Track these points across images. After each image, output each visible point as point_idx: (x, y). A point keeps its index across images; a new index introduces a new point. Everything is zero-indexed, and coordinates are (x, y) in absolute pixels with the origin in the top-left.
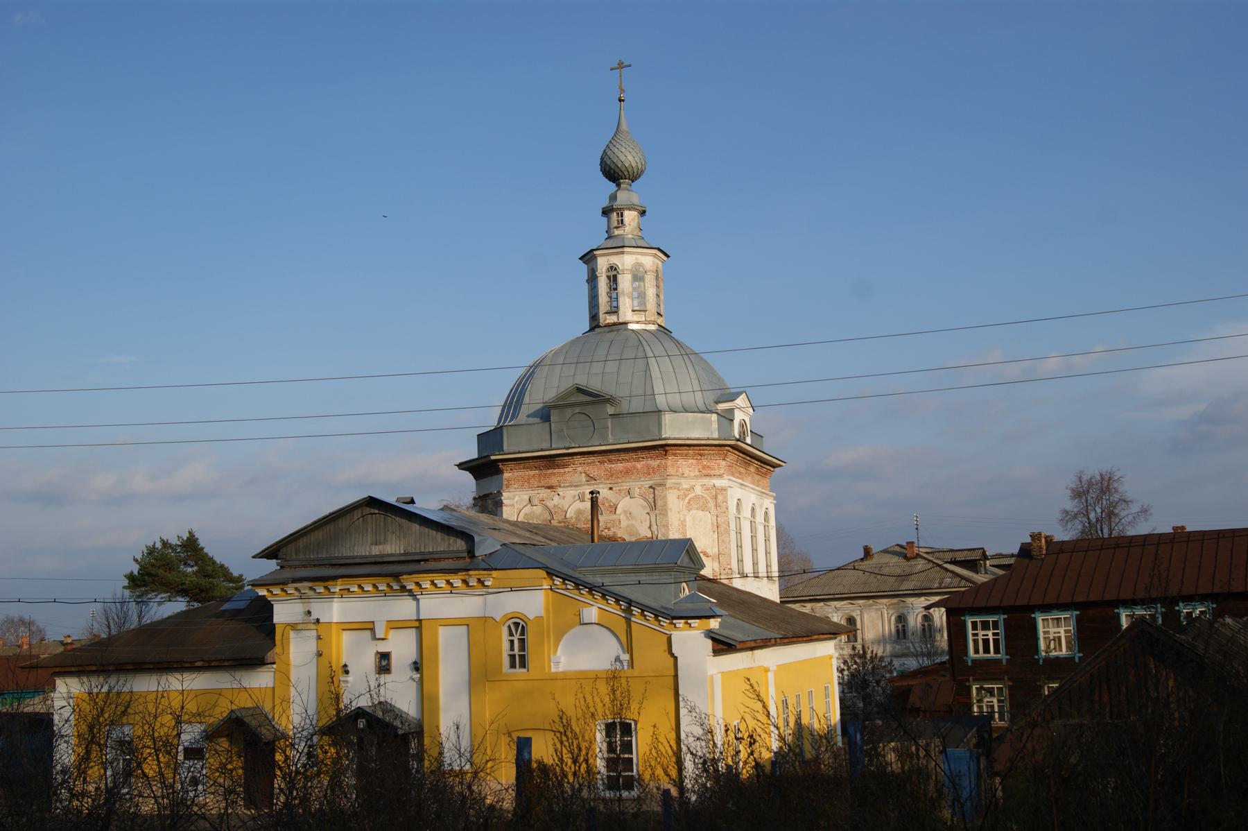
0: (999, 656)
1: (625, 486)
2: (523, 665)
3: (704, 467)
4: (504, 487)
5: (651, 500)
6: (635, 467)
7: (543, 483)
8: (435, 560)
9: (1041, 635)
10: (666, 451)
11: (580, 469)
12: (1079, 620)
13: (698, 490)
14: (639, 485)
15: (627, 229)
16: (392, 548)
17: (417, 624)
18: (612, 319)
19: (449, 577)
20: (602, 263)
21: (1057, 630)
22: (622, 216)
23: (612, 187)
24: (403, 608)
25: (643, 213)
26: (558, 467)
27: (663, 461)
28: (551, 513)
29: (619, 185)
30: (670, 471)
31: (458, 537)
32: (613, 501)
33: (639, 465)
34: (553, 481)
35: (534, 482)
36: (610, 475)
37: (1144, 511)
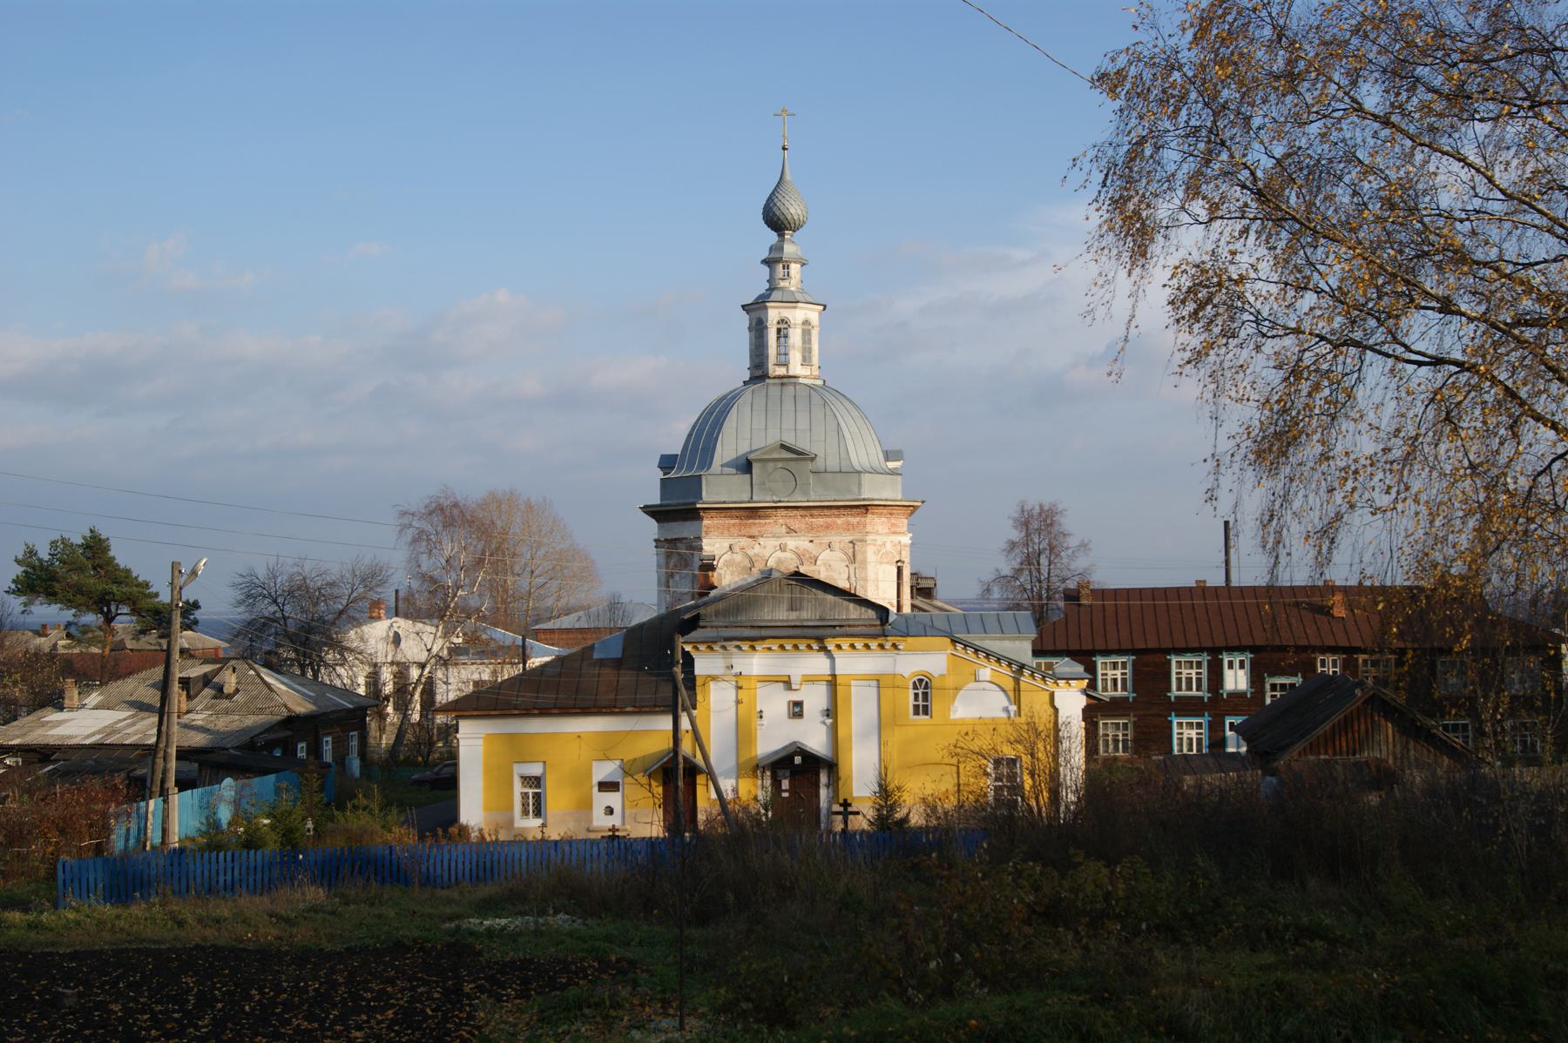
0: (1200, 694)
1: (826, 540)
2: (926, 712)
3: (893, 525)
4: (703, 534)
5: (851, 554)
6: (835, 523)
7: (743, 532)
8: (849, 626)
9: (1174, 677)
10: (867, 510)
11: (781, 521)
12: (1135, 664)
13: (889, 546)
14: (841, 539)
15: (793, 281)
16: (807, 615)
17: (830, 678)
18: (781, 371)
19: (867, 641)
20: (773, 315)
21: (1114, 672)
22: (788, 268)
23: (772, 237)
24: (816, 664)
25: (803, 265)
26: (760, 517)
27: (863, 519)
28: (751, 561)
29: (781, 235)
30: (869, 528)
31: (868, 607)
32: (814, 553)
33: (839, 521)
34: (754, 531)
35: (734, 530)
36: (811, 528)
37: (1084, 546)
